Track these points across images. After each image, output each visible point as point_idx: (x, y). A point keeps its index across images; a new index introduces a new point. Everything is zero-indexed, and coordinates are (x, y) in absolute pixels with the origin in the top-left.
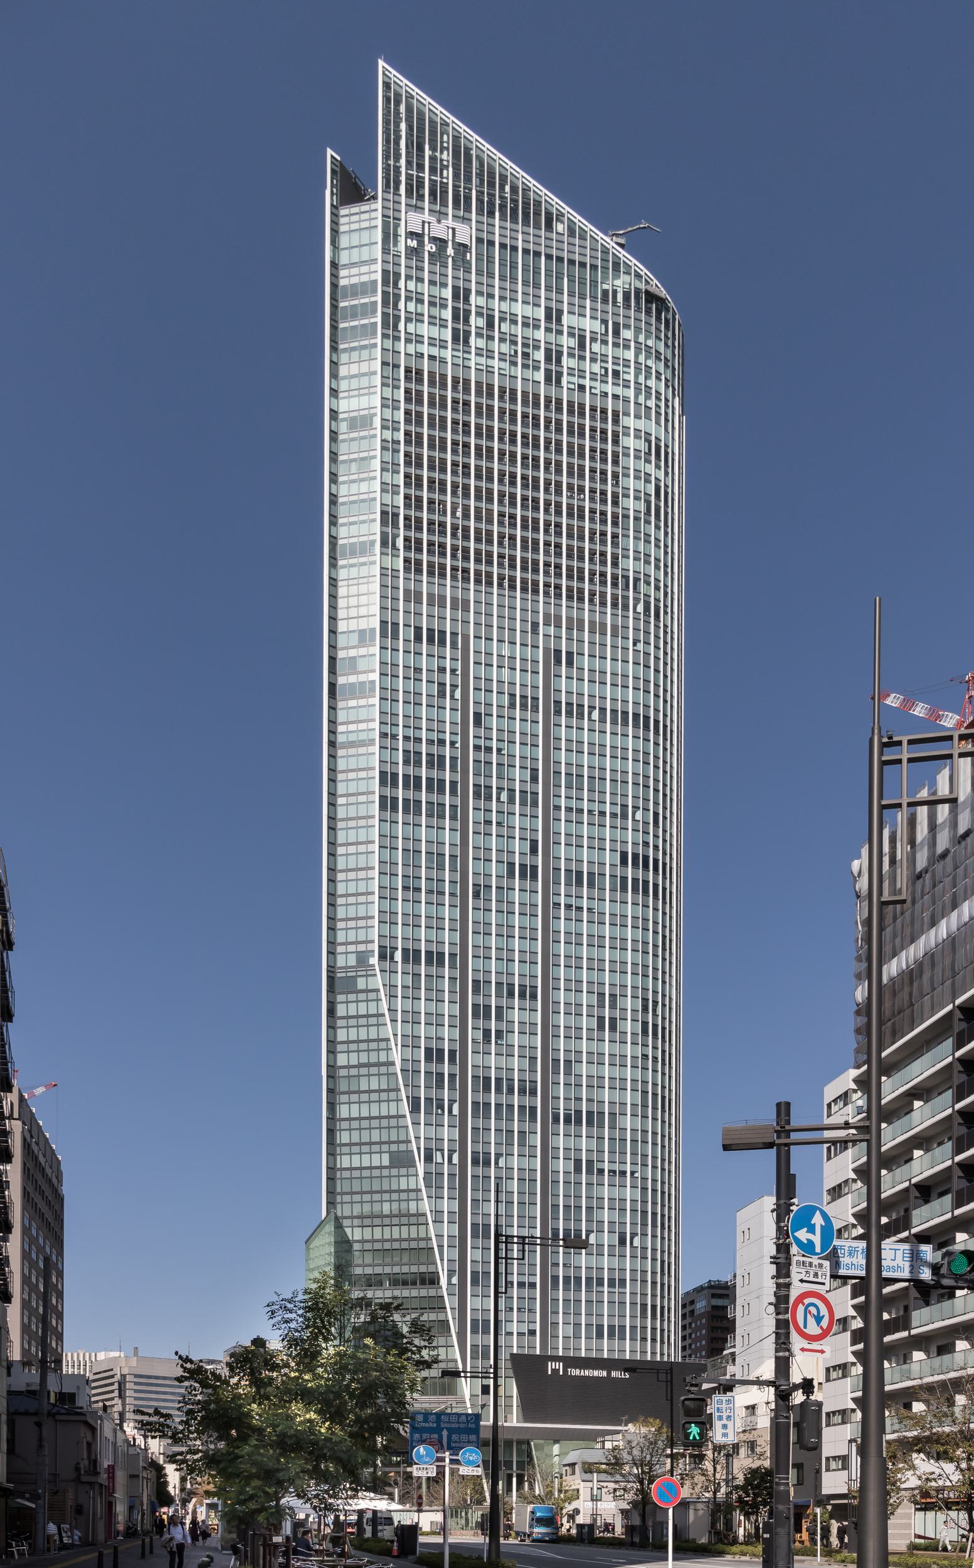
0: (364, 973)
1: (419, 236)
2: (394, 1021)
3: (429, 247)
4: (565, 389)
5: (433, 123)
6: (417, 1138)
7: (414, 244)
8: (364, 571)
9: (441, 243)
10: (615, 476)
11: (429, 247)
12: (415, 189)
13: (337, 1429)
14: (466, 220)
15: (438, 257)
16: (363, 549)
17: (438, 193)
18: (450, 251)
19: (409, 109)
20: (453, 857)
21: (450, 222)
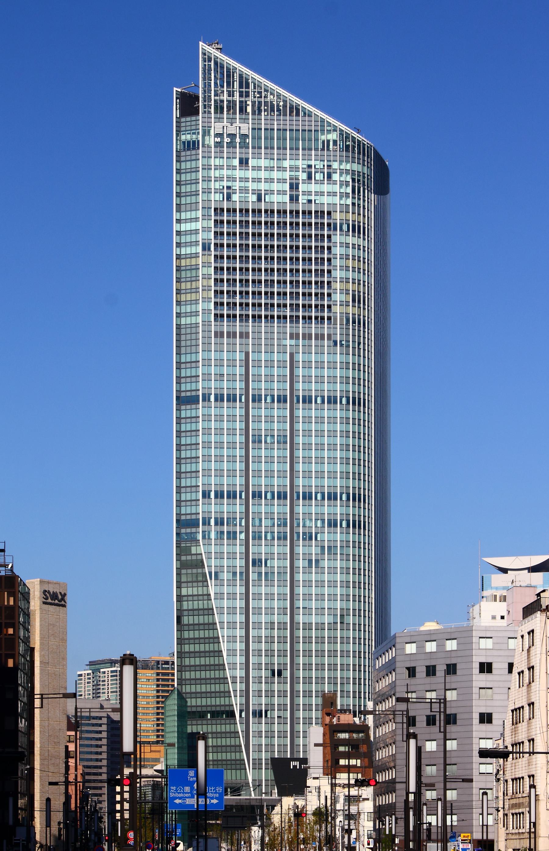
0: (195, 544)
3: (226, 140)
4: (301, 204)
5: (228, 70)
6: (223, 636)
7: (218, 140)
9: (232, 136)
10: (329, 260)
12: (219, 109)
14: (244, 120)
15: (232, 145)
18: (238, 140)
20: (241, 573)
21: (238, 124)
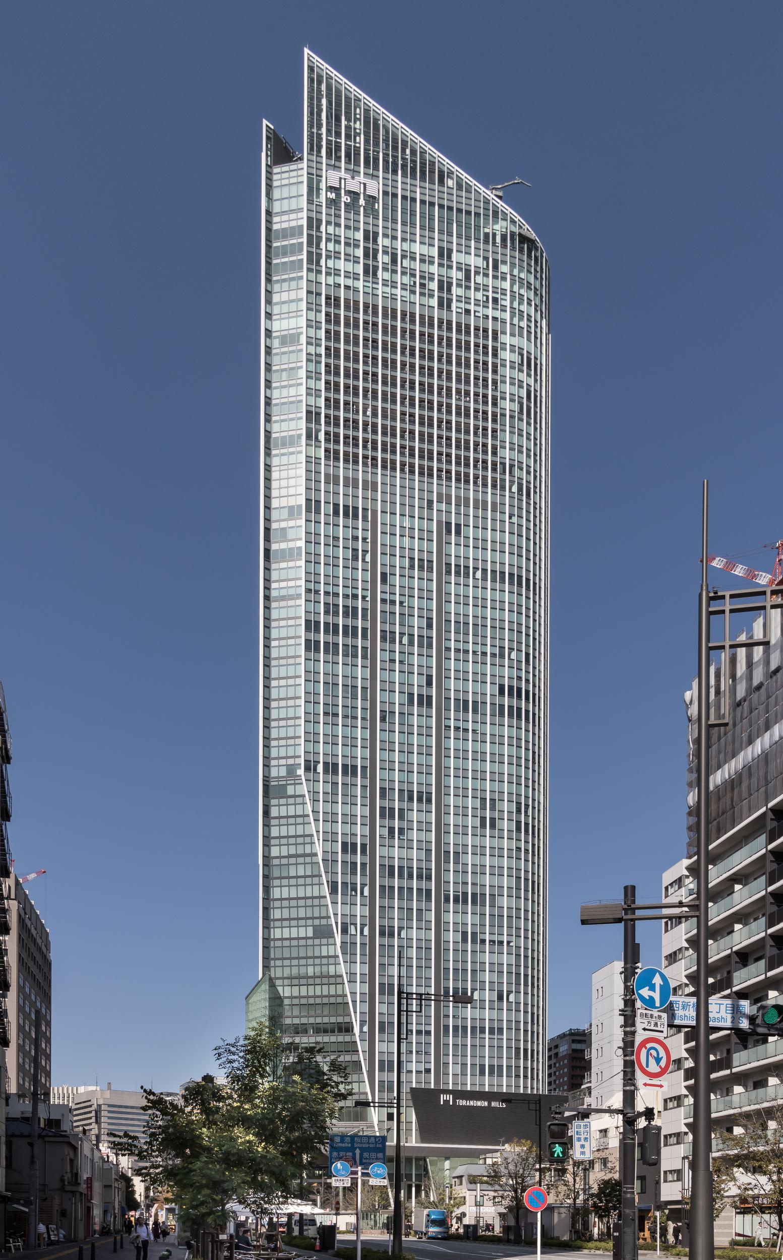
0: (293, 782)
1: (336, 190)
2: (317, 820)
3: (345, 199)
4: (454, 313)
5: (348, 99)
6: (336, 914)
7: (333, 196)
8: (293, 459)
9: (354, 195)
10: (495, 382)
11: (345, 199)
12: (333, 152)
13: (271, 1148)
14: (375, 177)
15: (352, 206)
16: (292, 441)
17: (352, 155)
18: (362, 202)
19: (329, 87)
20: (364, 689)
21: (362, 178)
